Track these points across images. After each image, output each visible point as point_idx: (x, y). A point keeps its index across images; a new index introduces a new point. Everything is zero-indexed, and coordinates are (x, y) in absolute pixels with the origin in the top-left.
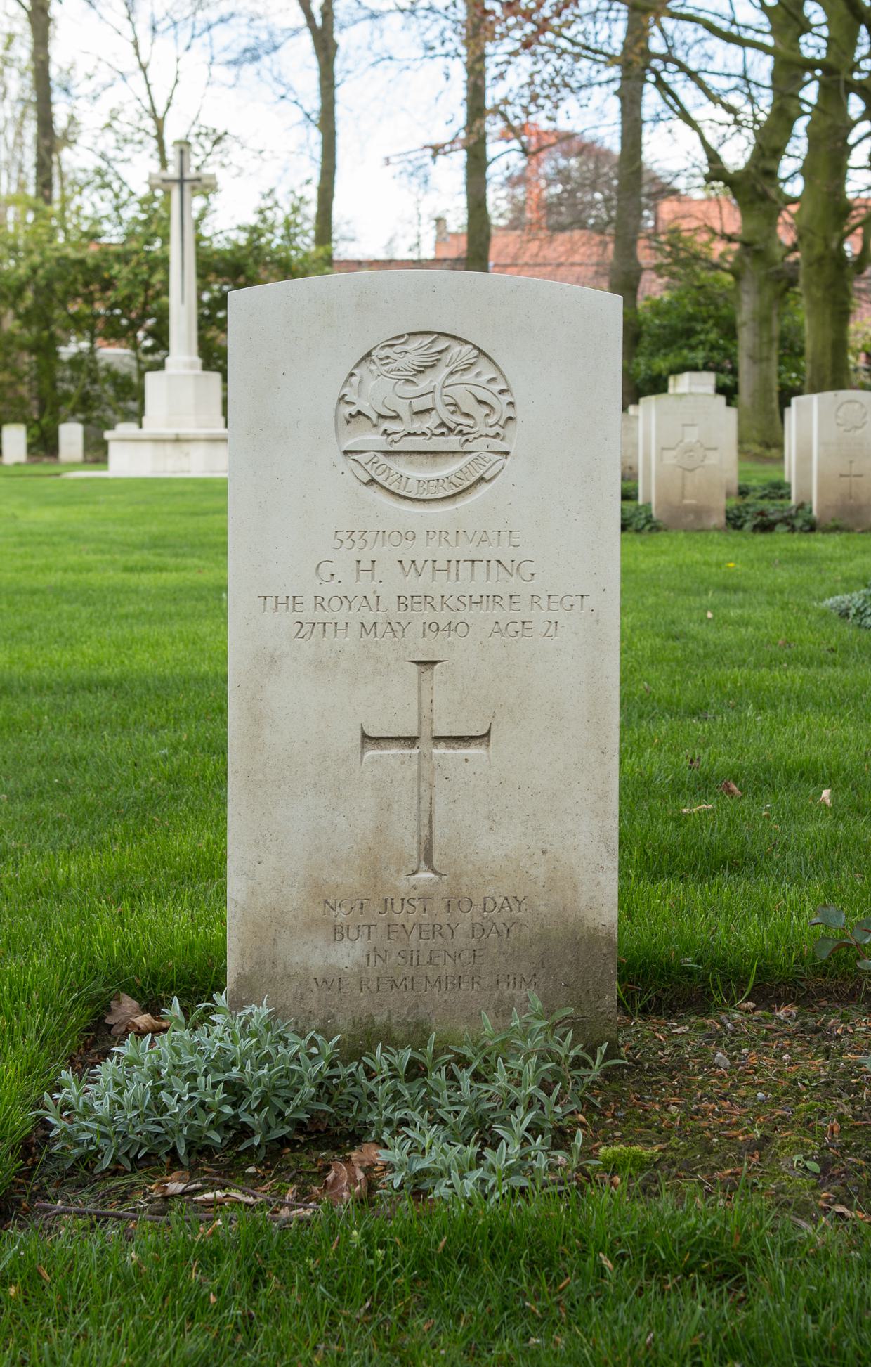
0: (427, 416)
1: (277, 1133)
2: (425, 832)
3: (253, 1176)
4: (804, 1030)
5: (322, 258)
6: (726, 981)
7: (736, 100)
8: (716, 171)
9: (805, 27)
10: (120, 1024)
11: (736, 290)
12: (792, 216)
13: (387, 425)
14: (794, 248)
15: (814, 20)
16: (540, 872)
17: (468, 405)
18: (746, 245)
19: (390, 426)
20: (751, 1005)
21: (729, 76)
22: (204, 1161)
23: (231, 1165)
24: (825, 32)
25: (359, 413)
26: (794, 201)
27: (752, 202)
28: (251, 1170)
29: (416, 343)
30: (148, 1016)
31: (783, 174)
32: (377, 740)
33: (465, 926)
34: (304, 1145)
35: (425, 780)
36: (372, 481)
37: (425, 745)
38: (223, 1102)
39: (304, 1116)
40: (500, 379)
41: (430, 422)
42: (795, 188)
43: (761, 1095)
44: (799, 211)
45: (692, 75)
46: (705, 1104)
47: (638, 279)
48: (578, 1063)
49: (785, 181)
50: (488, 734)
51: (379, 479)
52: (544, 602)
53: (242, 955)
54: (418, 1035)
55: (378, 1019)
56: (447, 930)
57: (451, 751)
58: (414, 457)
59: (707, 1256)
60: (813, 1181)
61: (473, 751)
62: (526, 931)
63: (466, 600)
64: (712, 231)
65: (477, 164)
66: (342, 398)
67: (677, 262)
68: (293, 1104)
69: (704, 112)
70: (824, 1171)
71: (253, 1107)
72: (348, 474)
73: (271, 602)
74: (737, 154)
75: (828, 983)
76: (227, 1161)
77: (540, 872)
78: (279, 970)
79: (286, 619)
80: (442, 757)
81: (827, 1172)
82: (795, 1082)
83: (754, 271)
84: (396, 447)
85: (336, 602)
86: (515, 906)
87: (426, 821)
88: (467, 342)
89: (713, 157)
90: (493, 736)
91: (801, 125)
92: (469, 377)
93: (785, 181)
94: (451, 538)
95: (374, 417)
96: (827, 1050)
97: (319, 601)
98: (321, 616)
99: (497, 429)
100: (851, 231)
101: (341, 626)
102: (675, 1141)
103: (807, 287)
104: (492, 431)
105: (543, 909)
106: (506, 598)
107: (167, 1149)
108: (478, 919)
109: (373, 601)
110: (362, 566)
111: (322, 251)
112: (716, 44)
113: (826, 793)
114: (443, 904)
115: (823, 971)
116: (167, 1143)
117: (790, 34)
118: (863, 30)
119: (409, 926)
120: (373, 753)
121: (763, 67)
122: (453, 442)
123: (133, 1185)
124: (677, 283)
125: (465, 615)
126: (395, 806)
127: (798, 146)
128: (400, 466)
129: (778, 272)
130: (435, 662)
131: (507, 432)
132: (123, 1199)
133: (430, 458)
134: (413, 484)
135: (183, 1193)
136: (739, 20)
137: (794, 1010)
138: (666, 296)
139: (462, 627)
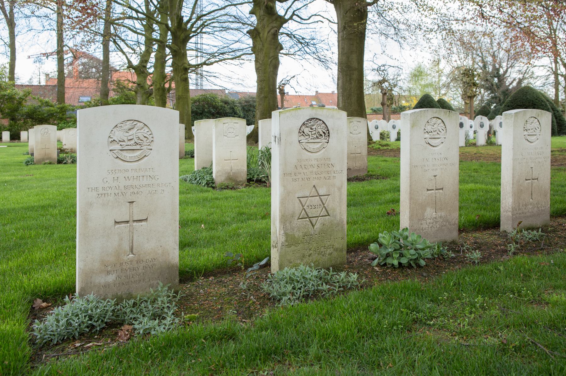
0: (131, 141)
1: (102, 326)
2: (131, 244)
3: (97, 338)
4: (217, 282)
5: (12, 84)
6: (197, 273)
7: (135, 47)
8: (130, 66)
9: (154, 30)
10: (37, 307)
11: (136, 96)
12: (151, 78)
13: (121, 143)
14: (152, 85)
15: (156, 29)
16: (160, 252)
17: (142, 138)
18: (139, 85)
19: (122, 143)
20: (203, 278)
21: (133, 41)
22: (82, 337)
23: (90, 337)
24: (159, 32)
25: (114, 140)
26: (151, 74)
27: (140, 74)
28: (96, 337)
29: (129, 122)
30: (45, 303)
31: (148, 67)
32: (118, 223)
33: (141, 267)
34: (107, 328)
35: (131, 232)
36: (117, 157)
37: (131, 223)
38: (88, 321)
39: (109, 321)
40: (150, 131)
41: (132, 142)
42: (151, 70)
43: (214, 298)
44: (153, 76)
45: (123, 40)
46: (203, 302)
47: (108, 93)
48: (174, 297)
49: (149, 68)
50: (147, 219)
51: (119, 157)
52: (161, 185)
53: (82, 282)
54: (130, 297)
55: (119, 294)
56: (137, 269)
57: (138, 224)
58: (128, 151)
59: (225, 335)
60: (236, 315)
61: (143, 223)
62: (157, 266)
63: (141, 186)
64: (129, 81)
65: (61, 61)
66: (109, 137)
67: (120, 88)
68: (106, 318)
69: (126, 49)
70: (238, 313)
71: (96, 320)
72: (111, 155)
73: (90, 189)
74: (135, 61)
75: (220, 270)
76: (89, 336)
77: (160, 252)
78: (92, 285)
79: (95, 193)
80: (135, 225)
81: (238, 314)
82: (221, 294)
83: (141, 91)
84: (124, 149)
85: (108, 188)
86: (154, 261)
87: (131, 242)
88: (440, 119)
89: (129, 62)
90: (148, 219)
91: (153, 55)
92: (142, 131)
93: (149, 68)
94: (138, 171)
95: (118, 141)
96: (225, 286)
97: (103, 188)
98: (104, 192)
99: (149, 143)
100: (167, 82)
101: (109, 194)
102: (200, 312)
103: (155, 96)
104: (148, 144)
105: (161, 261)
106: (151, 185)
107: (72, 336)
108: (145, 265)
109: (117, 187)
110: (115, 179)
111: (12, 82)
112: (130, 32)
113: (203, 225)
114: (136, 262)
115: (219, 268)
116: (72, 334)
117: (150, 32)
118: (169, 32)
119: (127, 269)
120: (117, 226)
121: (142, 39)
122: (438, 136)
123: (64, 347)
124: (119, 94)
125: (141, 189)
126: (123, 239)
127: (152, 59)
128: (124, 153)
129: (147, 92)
130: (133, 202)
131: (152, 144)
132: (63, 351)
133: (132, 151)
134: (312, 149)
135: (80, 346)
136: (136, 27)
137: (213, 278)
138: (116, 97)
139: (140, 193)
